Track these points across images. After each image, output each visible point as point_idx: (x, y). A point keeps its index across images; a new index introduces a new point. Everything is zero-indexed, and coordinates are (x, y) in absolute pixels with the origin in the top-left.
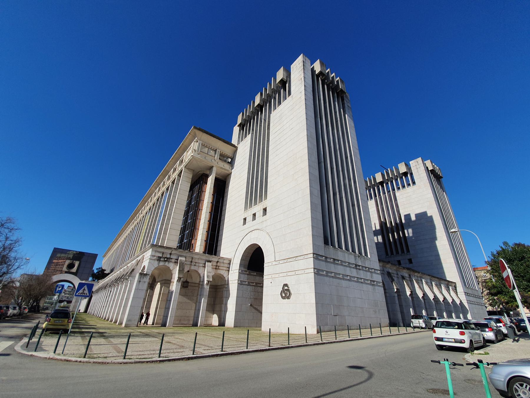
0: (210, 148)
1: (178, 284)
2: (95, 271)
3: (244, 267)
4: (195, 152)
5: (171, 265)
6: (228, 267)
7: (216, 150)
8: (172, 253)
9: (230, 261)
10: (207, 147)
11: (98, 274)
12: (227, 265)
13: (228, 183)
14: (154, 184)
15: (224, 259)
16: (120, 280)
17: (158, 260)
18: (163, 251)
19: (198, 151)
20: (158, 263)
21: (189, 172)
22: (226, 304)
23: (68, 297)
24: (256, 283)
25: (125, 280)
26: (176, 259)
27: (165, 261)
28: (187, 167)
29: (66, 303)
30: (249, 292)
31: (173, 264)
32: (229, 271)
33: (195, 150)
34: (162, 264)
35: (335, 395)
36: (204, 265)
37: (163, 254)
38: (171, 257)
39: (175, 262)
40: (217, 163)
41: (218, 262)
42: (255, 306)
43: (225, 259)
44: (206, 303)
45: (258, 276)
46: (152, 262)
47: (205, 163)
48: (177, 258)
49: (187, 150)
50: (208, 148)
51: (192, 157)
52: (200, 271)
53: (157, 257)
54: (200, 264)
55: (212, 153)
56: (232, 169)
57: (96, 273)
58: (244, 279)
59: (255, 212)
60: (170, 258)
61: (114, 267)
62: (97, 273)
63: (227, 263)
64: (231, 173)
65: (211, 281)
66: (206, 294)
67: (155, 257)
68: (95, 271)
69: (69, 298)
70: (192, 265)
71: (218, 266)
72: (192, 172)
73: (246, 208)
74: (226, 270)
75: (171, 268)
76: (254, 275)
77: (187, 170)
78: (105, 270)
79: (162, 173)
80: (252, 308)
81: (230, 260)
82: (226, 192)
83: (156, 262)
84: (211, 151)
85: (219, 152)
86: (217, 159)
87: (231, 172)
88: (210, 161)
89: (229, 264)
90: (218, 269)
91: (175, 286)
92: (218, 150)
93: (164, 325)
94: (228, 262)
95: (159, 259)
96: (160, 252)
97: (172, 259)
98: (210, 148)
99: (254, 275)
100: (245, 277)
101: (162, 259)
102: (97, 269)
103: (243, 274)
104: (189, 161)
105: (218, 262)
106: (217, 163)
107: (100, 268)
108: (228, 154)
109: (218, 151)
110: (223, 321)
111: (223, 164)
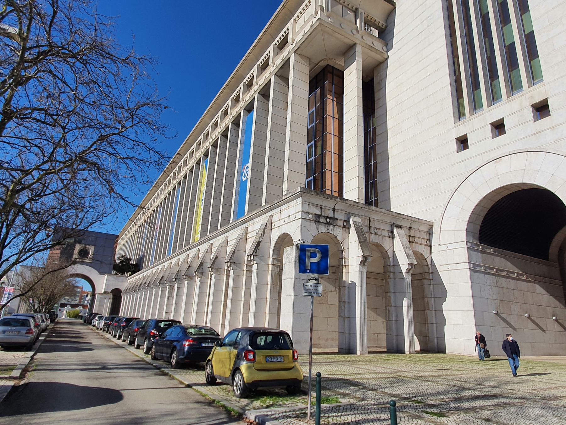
0: (345, 6)
1: (361, 270)
2: (118, 261)
3: (474, 237)
4: (322, 12)
5: (339, 232)
6: (428, 238)
7: (357, 9)
8: (335, 208)
9: (431, 227)
10: (341, 4)
11: (121, 266)
12: (426, 236)
13: (381, 80)
14: (211, 108)
15: (422, 223)
16: (212, 267)
17: (315, 221)
18: (321, 204)
19: (328, 11)
20: (317, 228)
21: (305, 64)
22: (439, 311)
23: (68, 300)
24: (498, 270)
25: (232, 265)
26: (345, 221)
27: (328, 224)
28: (299, 52)
29: (70, 307)
30: (489, 287)
31: (341, 230)
32: (431, 246)
33: (322, 9)
34: (323, 229)
35: (13, 354)
36: (390, 234)
37: (321, 208)
38: (336, 217)
39: (344, 227)
40: (362, 37)
41: (410, 228)
42: (502, 315)
43: (423, 222)
44: (412, 308)
45: (497, 256)
46: (307, 224)
47: (343, 37)
48: (346, 219)
49: (295, 16)
50: (342, 6)
51: (318, 22)
52: (386, 244)
53: (314, 215)
54: (383, 231)
55: (351, 15)
56: (387, 52)
57: (119, 264)
58: (477, 262)
59: (502, 117)
60: (334, 218)
61: (144, 255)
62: (120, 263)
63: (424, 232)
64: (387, 59)
65: (415, 265)
66: (409, 292)
67: (310, 216)
68: (118, 261)
69: (70, 300)
70: (371, 233)
71: (413, 237)
72: (308, 62)
73: (459, 113)
74: (425, 245)
75: (340, 238)
76: (491, 254)
77: (298, 58)
78: (130, 259)
79: (228, 83)
80: (499, 318)
81: (431, 224)
82: (379, 99)
83: (314, 225)
84: (348, 12)
85: (363, 13)
86: (361, 29)
87: (386, 57)
88: (350, 32)
89: (428, 232)
90: (413, 242)
91: (187, 285)
92: (360, 10)
93: (368, 348)
94: (424, 228)
95: (317, 219)
96: (316, 206)
97: (337, 219)
98: (345, 6)
99: (491, 254)
100: (478, 258)
101: (322, 220)
102: (119, 258)
103: (474, 251)
104: (304, 39)
105: (410, 228)
106: (362, 37)
107: (122, 257)
108: (378, 20)
109: (361, 13)
110: (397, 340)
111: (371, 39)
